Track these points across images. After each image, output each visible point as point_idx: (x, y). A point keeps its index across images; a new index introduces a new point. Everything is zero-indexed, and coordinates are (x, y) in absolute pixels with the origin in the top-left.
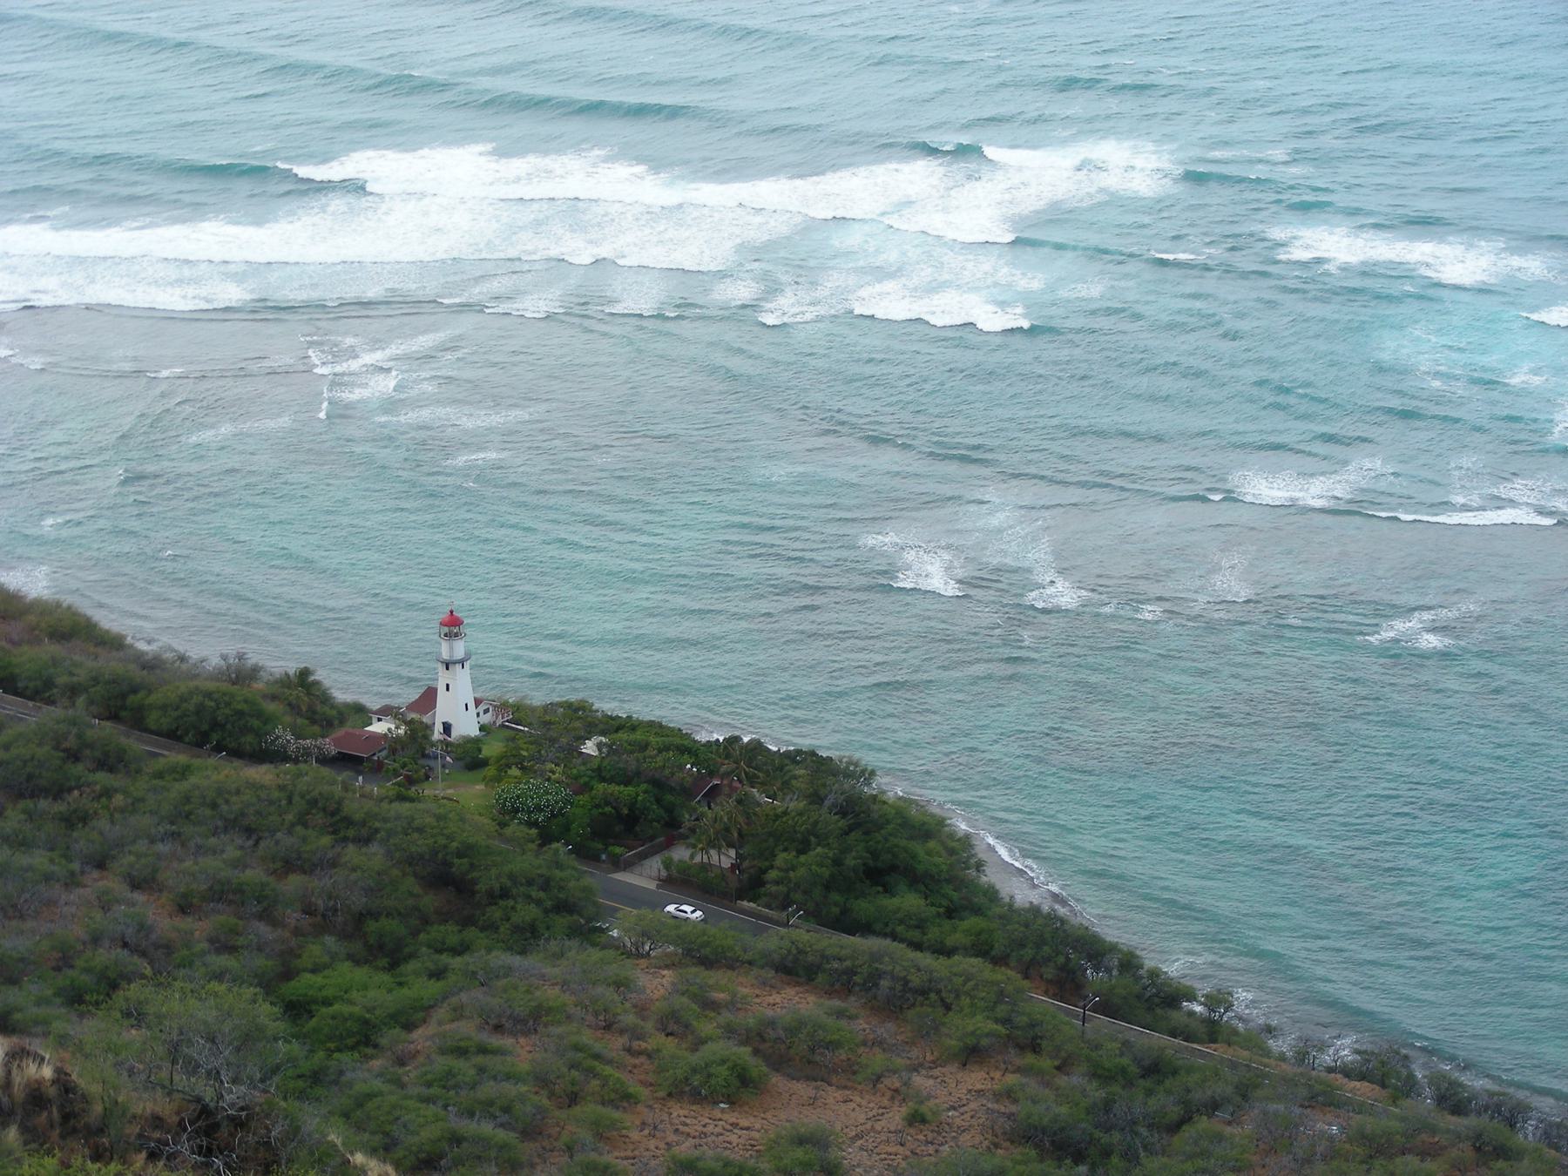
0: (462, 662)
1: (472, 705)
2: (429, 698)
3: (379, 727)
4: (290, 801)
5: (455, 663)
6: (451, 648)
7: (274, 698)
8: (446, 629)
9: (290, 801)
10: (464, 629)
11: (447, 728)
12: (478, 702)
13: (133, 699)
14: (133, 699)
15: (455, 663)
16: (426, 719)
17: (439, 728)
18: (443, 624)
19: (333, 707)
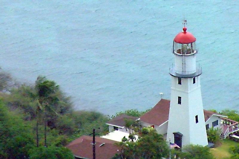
0: (193, 77)
1: (201, 118)
2: (163, 108)
3: (117, 136)
4: (72, 3)
5: (187, 77)
6: (184, 64)
7: (17, 104)
8: (179, 46)
9: (72, 3)
10: (198, 44)
11: (178, 138)
12: (207, 115)
13: (21, 149)
14: (21, 149)
15: (187, 77)
16: (159, 130)
17: (170, 138)
18: (177, 40)
19: (71, 115)
